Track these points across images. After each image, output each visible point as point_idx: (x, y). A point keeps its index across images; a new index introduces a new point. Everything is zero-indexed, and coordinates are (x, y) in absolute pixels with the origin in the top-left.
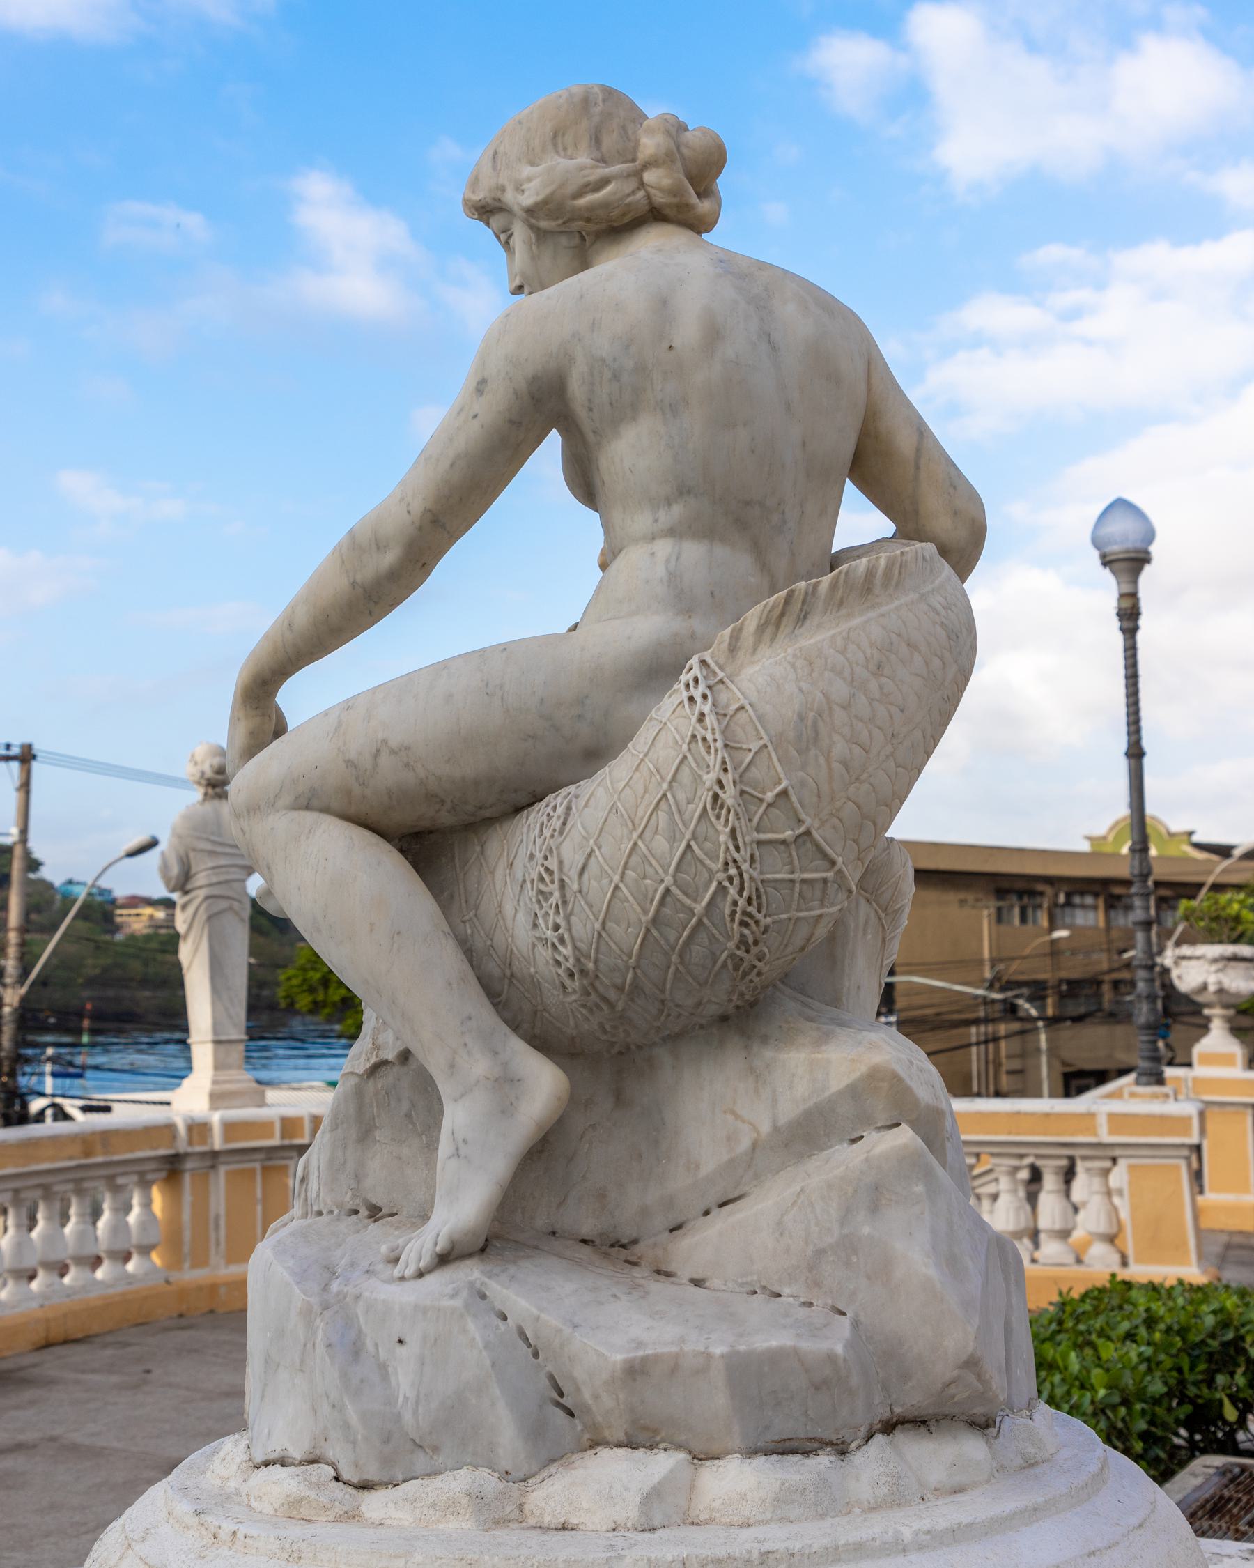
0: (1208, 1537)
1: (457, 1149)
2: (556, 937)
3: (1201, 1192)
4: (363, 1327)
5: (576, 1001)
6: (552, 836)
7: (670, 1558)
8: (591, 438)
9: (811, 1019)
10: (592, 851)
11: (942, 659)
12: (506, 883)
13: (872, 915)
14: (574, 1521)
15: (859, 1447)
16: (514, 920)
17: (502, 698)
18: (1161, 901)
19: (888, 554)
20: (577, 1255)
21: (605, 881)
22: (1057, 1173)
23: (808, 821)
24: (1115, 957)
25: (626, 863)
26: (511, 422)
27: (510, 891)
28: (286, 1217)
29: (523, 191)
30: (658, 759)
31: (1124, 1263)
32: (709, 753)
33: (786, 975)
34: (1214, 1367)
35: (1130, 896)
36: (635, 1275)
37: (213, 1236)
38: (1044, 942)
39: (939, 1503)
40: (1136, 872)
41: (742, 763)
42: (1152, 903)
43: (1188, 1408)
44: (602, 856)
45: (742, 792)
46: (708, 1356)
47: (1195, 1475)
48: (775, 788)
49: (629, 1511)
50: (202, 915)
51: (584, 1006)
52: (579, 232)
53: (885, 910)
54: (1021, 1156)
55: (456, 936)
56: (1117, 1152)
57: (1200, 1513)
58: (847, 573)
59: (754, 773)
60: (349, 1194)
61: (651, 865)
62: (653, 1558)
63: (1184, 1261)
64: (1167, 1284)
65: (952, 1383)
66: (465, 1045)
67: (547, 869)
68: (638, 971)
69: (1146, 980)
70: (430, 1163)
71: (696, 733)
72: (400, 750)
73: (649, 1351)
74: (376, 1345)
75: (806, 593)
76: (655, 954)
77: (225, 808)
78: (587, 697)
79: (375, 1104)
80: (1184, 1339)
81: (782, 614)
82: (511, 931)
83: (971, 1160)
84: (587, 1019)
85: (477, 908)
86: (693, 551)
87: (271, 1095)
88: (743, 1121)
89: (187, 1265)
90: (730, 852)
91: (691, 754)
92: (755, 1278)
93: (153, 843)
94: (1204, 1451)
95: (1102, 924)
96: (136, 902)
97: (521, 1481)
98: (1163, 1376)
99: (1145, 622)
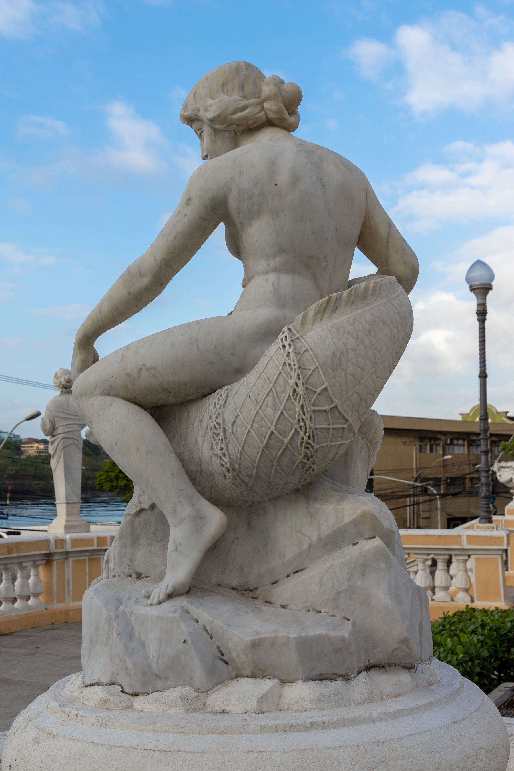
0: (505, 717)
1: (176, 548)
2: (222, 453)
3: (507, 570)
5: (230, 482)
6: (220, 408)
7: (270, 725)
8: (239, 226)
9: (336, 491)
10: (238, 415)
11: (398, 329)
12: (199, 429)
13: (364, 444)
14: (228, 709)
15: (354, 677)
16: (202, 446)
17: (197, 345)
18: (493, 443)
19: (374, 281)
20: (230, 595)
21: (244, 428)
22: (444, 562)
23: (336, 402)
24: (472, 467)
25: (254, 420)
26: (202, 218)
27: (201, 433)
28: (99, 578)
29: (208, 111)
30: (268, 374)
31: (472, 601)
32: (292, 370)
33: (325, 471)
34: (510, 645)
35: (479, 440)
36: (256, 603)
37: (66, 589)
38: (441, 460)
39: (389, 701)
40: (482, 429)
41: (306, 375)
42: (489, 443)
43: (498, 663)
44: (243, 417)
45: (307, 389)
46: (288, 638)
47: (500, 691)
48: (321, 387)
49: (252, 705)
50: (61, 447)
51: (234, 484)
52: (234, 131)
53: (370, 443)
54: (429, 554)
55: (176, 453)
56: (470, 553)
57: (502, 707)
58: (355, 289)
59: (312, 380)
60: (128, 568)
61: (265, 421)
62: (263, 725)
63: (499, 600)
64: (491, 609)
65: (396, 649)
66: (180, 501)
67: (218, 423)
68: (259, 469)
69: (485, 477)
70: (164, 554)
71: (286, 361)
72: (151, 369)
74: (140, 634)
75: (337, 298)
76: (266, 461)
77: (71, 398)
78: (236, 345)
79: (139, 528)
80: (498, 633)
81: (326, 308)
82: (201, 451)
83: (406, 556)
84: (236, 491)
85: (185, 440)
86: (285, 279)
87: (92, 527)
88: (305, 536)
89: (55, 602)
90: (301, 415)
91: (284, 371)
92: (309, 604)
93: (38, 415)
94: (505, 681)
95: (466, 453)
96: (31, 441)
97: (205, 692)
98: (488, 649)
99: (489, 317)
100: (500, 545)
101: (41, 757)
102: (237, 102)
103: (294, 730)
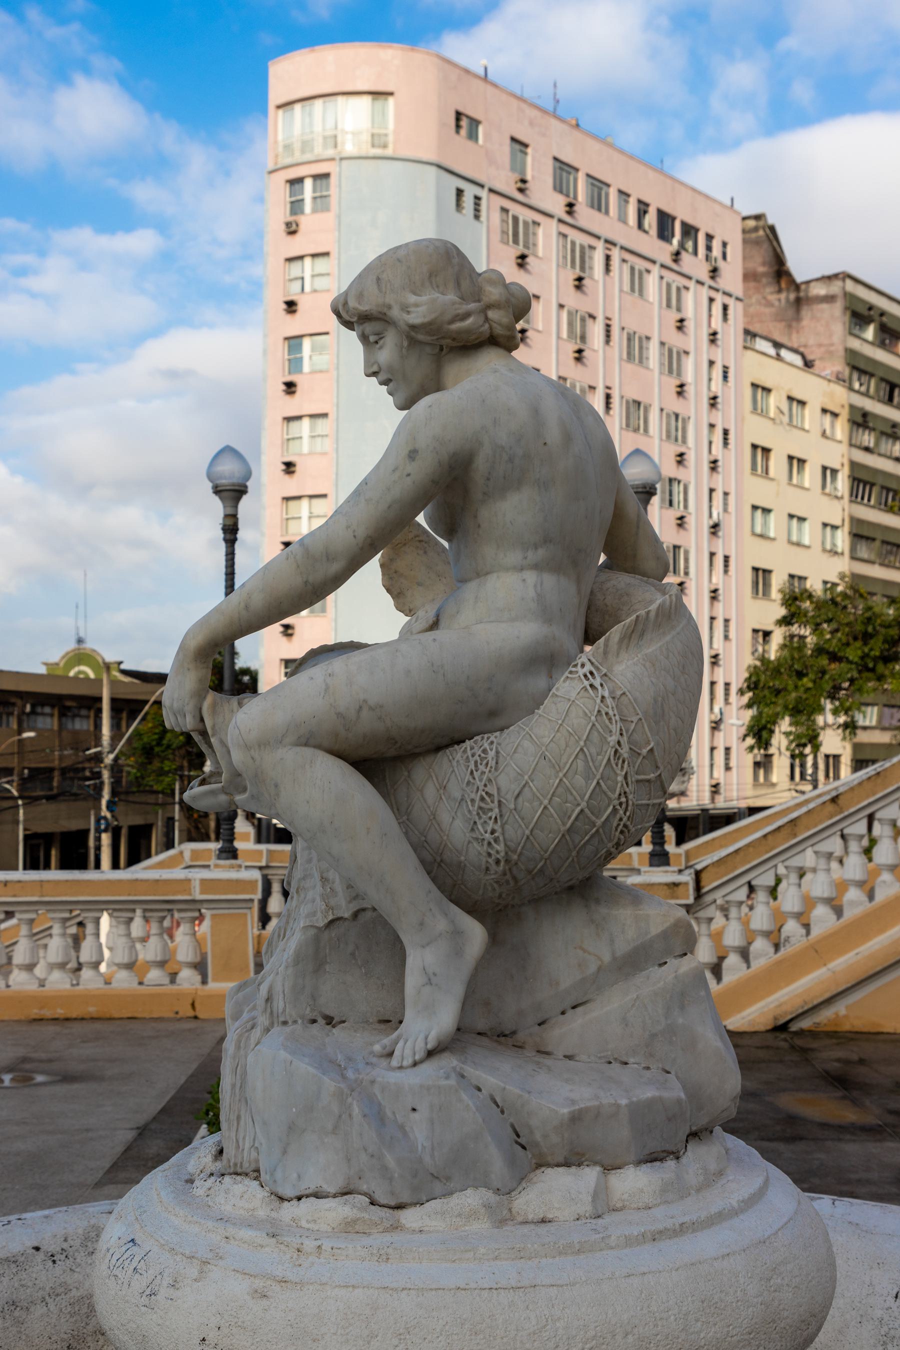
1: (429, 980)
4: (382, 1102)
7: (636, 1234)
10: (527, 783)
15: (684, 1153)
16: (451, 825)
21: (536, 804)
26: (433, 481)
32: (611, 723)
46: (618, 1106)
49: (586, 1208)
60: (308, 1009)
61: (572, 794)
66: (431, 910)
67: (487, 793)
73: (582, 1106)
74: (394, 1113)
79: (328, 947)
86: (549, 580)
88: (590, 954)
92: (609, 1053)
95: (56, 727)
100: (252, 893)
101: (287, 1319)
102: (457, 306)
103: (664, 1237)
